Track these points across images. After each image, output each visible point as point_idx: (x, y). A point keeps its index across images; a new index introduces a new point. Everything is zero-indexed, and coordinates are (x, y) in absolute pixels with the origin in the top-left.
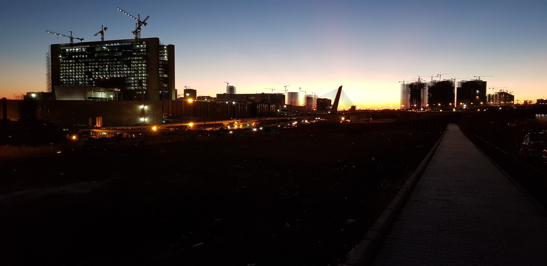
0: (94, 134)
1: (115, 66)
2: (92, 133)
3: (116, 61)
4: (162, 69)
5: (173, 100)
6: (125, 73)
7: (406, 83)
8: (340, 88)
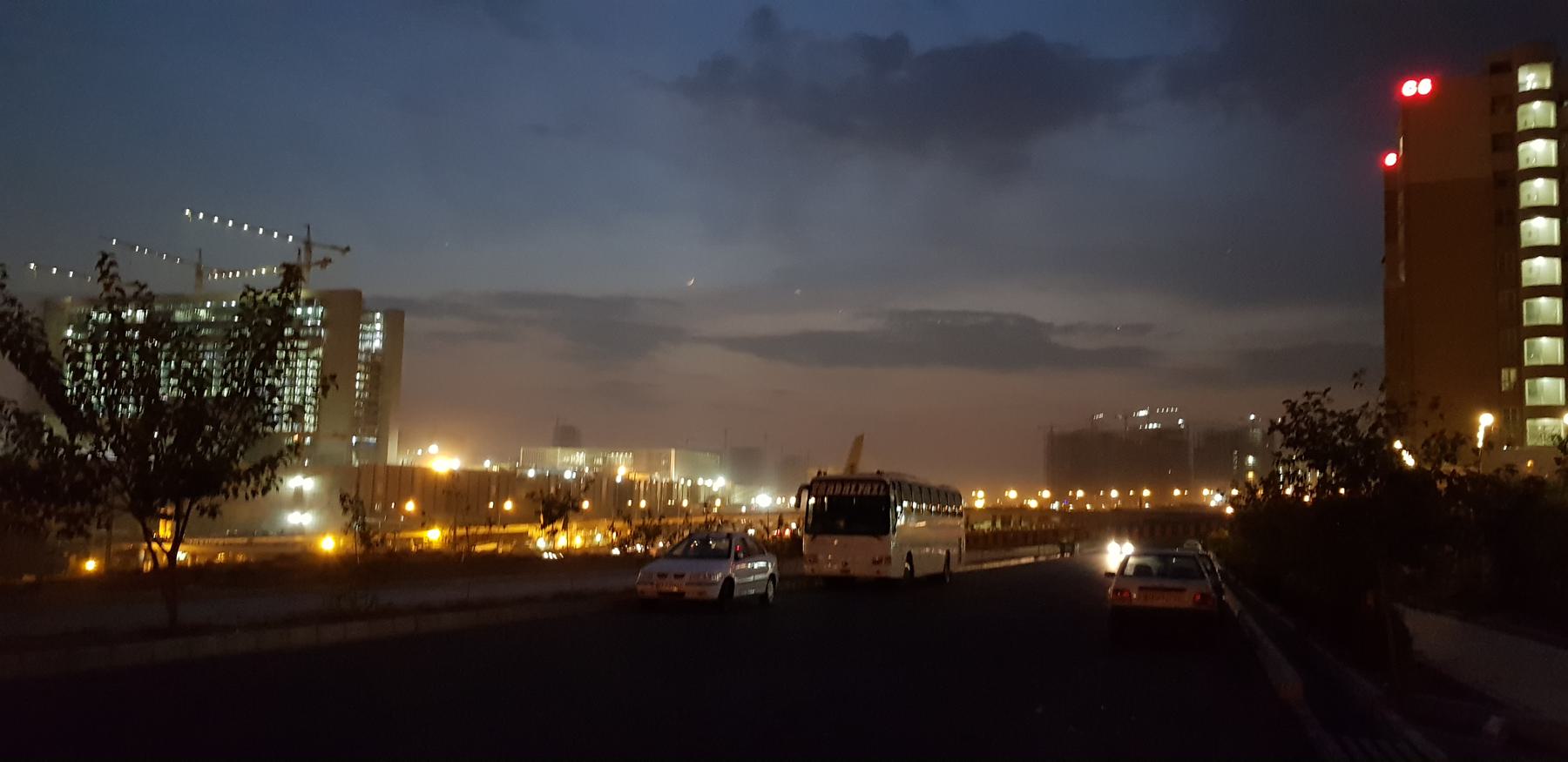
7: (1056, 430)
8: (859, 441)
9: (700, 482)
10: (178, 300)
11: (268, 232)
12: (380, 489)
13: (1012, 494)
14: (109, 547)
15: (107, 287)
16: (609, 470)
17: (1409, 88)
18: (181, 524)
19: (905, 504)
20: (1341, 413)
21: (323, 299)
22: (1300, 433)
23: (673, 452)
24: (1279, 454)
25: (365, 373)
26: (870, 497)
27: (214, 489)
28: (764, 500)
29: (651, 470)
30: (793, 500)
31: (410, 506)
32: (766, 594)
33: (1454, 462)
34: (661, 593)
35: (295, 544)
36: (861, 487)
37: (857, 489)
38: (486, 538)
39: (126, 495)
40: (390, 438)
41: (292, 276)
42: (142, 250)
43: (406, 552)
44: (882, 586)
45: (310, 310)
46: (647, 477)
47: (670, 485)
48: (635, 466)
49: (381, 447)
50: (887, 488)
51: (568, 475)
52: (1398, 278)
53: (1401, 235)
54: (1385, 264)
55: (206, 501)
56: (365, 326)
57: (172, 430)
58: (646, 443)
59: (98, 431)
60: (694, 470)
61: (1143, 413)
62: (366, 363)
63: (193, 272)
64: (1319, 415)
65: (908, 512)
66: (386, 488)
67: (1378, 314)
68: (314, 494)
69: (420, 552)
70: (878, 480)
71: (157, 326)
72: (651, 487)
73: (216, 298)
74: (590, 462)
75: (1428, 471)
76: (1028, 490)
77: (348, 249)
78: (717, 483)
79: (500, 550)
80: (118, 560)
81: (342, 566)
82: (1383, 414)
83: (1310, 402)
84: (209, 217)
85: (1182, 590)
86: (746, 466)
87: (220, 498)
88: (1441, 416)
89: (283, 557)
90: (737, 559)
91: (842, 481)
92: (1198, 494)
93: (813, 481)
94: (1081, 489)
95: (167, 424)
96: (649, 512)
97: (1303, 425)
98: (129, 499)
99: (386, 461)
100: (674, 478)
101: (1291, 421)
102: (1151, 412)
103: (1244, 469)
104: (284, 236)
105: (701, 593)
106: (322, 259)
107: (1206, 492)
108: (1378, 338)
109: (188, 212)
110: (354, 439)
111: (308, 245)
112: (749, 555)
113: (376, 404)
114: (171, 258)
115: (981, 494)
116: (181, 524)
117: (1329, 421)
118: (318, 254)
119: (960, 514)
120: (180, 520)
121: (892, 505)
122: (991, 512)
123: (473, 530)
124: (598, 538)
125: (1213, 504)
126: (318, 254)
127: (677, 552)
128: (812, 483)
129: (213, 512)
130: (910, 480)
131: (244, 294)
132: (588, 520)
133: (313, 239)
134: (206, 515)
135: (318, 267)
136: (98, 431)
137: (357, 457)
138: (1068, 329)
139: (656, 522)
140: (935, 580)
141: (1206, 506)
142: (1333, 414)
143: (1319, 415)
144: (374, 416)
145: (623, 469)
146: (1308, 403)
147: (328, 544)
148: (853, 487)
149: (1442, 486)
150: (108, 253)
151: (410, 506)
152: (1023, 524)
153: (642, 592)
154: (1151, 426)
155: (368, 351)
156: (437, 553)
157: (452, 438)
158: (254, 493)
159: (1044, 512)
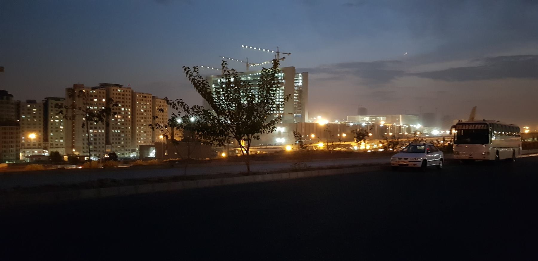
9: (411, 126)
10: (242, 73)
11: (262, 49)
12: (303, 131)
14: (228, 149)
16: (378, 122)
18: (249, 142)
21: (284, 71)
28: (436, 132)
29: (392, 122)
30: (448, 132)
32: (439, 165)
34: (399, 165)
35: (279, 148)
37: (475, 127)
38: (338, 146)
39: (234, 133)
41: (276, 63)
43: (312, 150)
44: (486, 163)
45: (280, 74)
46: (391, 125)
47: (400, 127)
48: (387, 121)
49: (303, 117)
55: (256, 135)
56: (296, 79)
59: (226, 115)
60: (408, 121)
63: (246, 64)
65: (497, 135)
69: (317, 150)
70: (484, 123)
71: (237, 82)
72: (393, 128)
74: (371, 120)
77: (290, 54)
80: (231, 153)
81: (294, 156)
84: (249, 47)
87: (259, 134)
89: (276, 152)
90: (428, 153)
91: (469, 124)
93: (457, 124)
95: (243, 112)
96: (393, 137)
98: (235, 135)
100: (401, 124)
104: (271, 51)
105: (457, 157)
106: (282, 58)
109: (243, 46)
112: (432, 152)
113: (301, 103)
114: (239, 61)
116: (249, 142)
118: (281, 56)
120: (248, 140)
121: (490, 133)
123: (334, 143)
126: (281, 56)
130: (497, 123)
131: (262, 71)
132: (372, 139)
134: (256, 139)
135: (37, 101)
136: (226, 115)
137: (296, 120)
139: (396, 140)
140: (508, 161)
144: (300, 107)
145: (382, 122)
147: (289, 148)
148: (474, 126)
150: (72, 87)
151: (308, 136)
153: (393, 164)
155: (297, 86)
156: (323, 151)
157: (325, 114)
158: (269, 132)
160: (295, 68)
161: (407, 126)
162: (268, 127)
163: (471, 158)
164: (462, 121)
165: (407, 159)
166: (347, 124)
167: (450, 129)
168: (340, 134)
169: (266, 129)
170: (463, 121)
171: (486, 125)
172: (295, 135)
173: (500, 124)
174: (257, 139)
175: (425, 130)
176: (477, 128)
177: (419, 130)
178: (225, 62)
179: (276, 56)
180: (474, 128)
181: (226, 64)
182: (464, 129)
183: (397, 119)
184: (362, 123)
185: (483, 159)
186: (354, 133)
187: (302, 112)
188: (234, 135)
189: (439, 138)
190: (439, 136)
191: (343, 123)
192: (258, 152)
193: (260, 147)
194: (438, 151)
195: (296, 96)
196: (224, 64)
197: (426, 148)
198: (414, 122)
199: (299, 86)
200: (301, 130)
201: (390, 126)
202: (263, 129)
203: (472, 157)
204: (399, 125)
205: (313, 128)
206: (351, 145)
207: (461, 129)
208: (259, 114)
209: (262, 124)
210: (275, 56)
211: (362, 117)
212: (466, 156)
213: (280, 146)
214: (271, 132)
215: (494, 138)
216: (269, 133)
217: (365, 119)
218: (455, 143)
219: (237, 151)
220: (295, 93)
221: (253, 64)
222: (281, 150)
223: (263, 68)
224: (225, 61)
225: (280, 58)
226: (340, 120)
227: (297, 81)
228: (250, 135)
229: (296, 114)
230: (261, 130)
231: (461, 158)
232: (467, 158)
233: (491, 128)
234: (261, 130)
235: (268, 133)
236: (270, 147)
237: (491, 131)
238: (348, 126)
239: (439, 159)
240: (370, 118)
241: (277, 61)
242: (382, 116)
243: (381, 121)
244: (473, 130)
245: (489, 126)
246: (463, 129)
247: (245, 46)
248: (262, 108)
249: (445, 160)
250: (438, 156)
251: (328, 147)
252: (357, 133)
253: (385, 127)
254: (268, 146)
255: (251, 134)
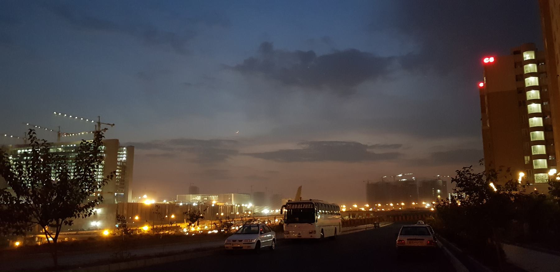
0: (40, 240)
1: (69, 167)
2: (37, 238)
3: (71, 163)
4: (119, 171)
5: (128, 203)
6: (99, 174)
7: (370, 182)
8: (300, 188)
9: (243, 205)
13: (355, 206)
15: (32, 141)
16: (210, 201)
17: (486, 60)
19: (320, 211)
20: (473, 174)
22: (463, 182)
23: (233, 194)
24: (455, 190)
25: (120, 169)
26: (308, 209)
27: (71, 215)
28: (266, 211)
29: (224, 202)
31: (137, 218)
33: (516, 190)
36: (304, 205)
37: (303, 206)
38: (166, 229)
39: (39, 218)
40: (129, 192)
41: (98, 136)
42: (38, 127)
47: (232, 206)
48: (219, 200)
49: (126, 196)
50: (313, 206)
51: (194, 204)
52: (487, 126)
53: (487, 110)
54: (481, 121)
55: (68, 219)
56: (120, 153)
57: (56, 193)
58: (223, 192)
60: (240, 200)
61: (400, 175)
62: (120, 166)
63: (57, 134)
64: (469, 176)
66: (127, 212)
67: (481, 139)
68: (101, 215)
70: (310, 203)
72: (225, 207)
73: (65, 144)
74: (202, 199)
75: (507, 194)
76: (361, 204)
78: (249, 205)
79: (170, 233)
82: (491, 174)
83: (465, 171)
84: (63, 114)
85: (423, 240)
86: (260, 199)
87: (73, 218)
88: (511, 174)
89: (91, 239)
90: (261, 234)
91: (297, 204)
92: (421, 204)
93: (287, 204)
94: (392, 203)
97: (463, 179)
98: (39, 220)
99: (127, 201)
100: (233, 204)
101: (459, 178)
102: (403, 175)
103: (437, 194)
105: (288, 237)
106: (104, 128)
107: (424, 203)
108: (480, 147)
110: (116, 194)
111: (99, 123)
112: (266, 233)
113: (124, 181)
114: (49, 130)
115: (344, 206)
117: (472, 178)
118: (103, 127)
119: (339, 214)
121: (316, 212)
122: (348, 213)
124: (206, 227)
125: (426, 207)
127: (239, 232)
128: (286, 204)
129: (70, 223)
130: (322, 202)
133: (101, 121)
134: (68, 224)
137: (117, 201)
138: (373, 147)
141: (424, 208)
142: (473, 175)
143: (469, 176)
144: (123, 185)
146: (464, 171)
147: (106, 233)
148: (301, 205)
149: (513, 199)
151: (137, 218)
152: (360, 217)
154: (403, 180)
155: (121, 161)
157: (152, 192)
158: (86, 215)
159: (367, 212)
160: (119, 141)
161: (239, 206)
162: (85, 209)
163: (300, 238)
164: (291, 200)
165: (241, 241)
166: (176, 204)
167: (281, 209)
168: (140, 219)
169: (82, 212)
170: (292, 201)
171: (312, 205)
172: (118, 219)
173: (323, 203)
174: (69, 225)
175: (256, 210)
176: (305, 207)
177: (250, 210)
178: (33, 131)
179: (96, 126)
180: (302, 208)
181: (34, 133)
182: (293, 208)
183: (229, 198)
184: (193, 203)
185: (311, 238)
186: (187, 215)
187: (125, 191)
188: (38, 220)
189: (269, 217)
190: (269, 215)
191: (172, 203)
192: (66, 239)
193: (68, 233)
194: (271, 231)
195: (118, 172)
196: (32, 133)
197: (259, 229)
198: (246, 202)
199: (123, 161)
200: (123, 212)
201: (222, 206)
202: (78, 213)
203: (301, 236)
204: (231, 205)
205: (137, 209)
206: (181, 228)
207: (290, 208)
208: (74, 194)
209: (78, 206)
210: (95, 126)
211: (193, 196)
212: (295, 236)
213: (95, 231)
214: (88, 215)
215: (319, 217)
216: (85, 217)
217: (196, 198)
218: (285, 223)
219: (37, 239)
220: (118, 169)
221: (67, 134)
222: (96, 236)
223: (83, 140)
224: (33, 130)
225: (101, 129)
226: (168, 200)
227: (121, 156)
228: (61, 220)
229: (116, 193)
230: (75, 213)
231: (291, 238)
232: (297, 237)
233: (317, 207)
234: (75, 213)
235: (84, 216)
236: (82, 232)
237: (316, 210)
238: (178, 206)
239: (272, 239)
240: (203, 197)
241: (101, 133)
242: (215, 196)
243: (213, 200)
244: (300, 209)
245: (315, 205)
246: (292, 208)
247: (57, 113)
248: (79, 188)
249: (277, 240)
250: (270, 236)
251: (153, 229)
252: (190, 215)
253: (217, 207)
254: (79, 231)
255: (61, 218)
